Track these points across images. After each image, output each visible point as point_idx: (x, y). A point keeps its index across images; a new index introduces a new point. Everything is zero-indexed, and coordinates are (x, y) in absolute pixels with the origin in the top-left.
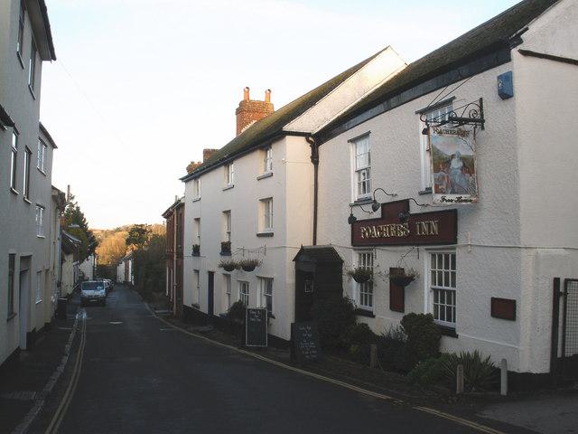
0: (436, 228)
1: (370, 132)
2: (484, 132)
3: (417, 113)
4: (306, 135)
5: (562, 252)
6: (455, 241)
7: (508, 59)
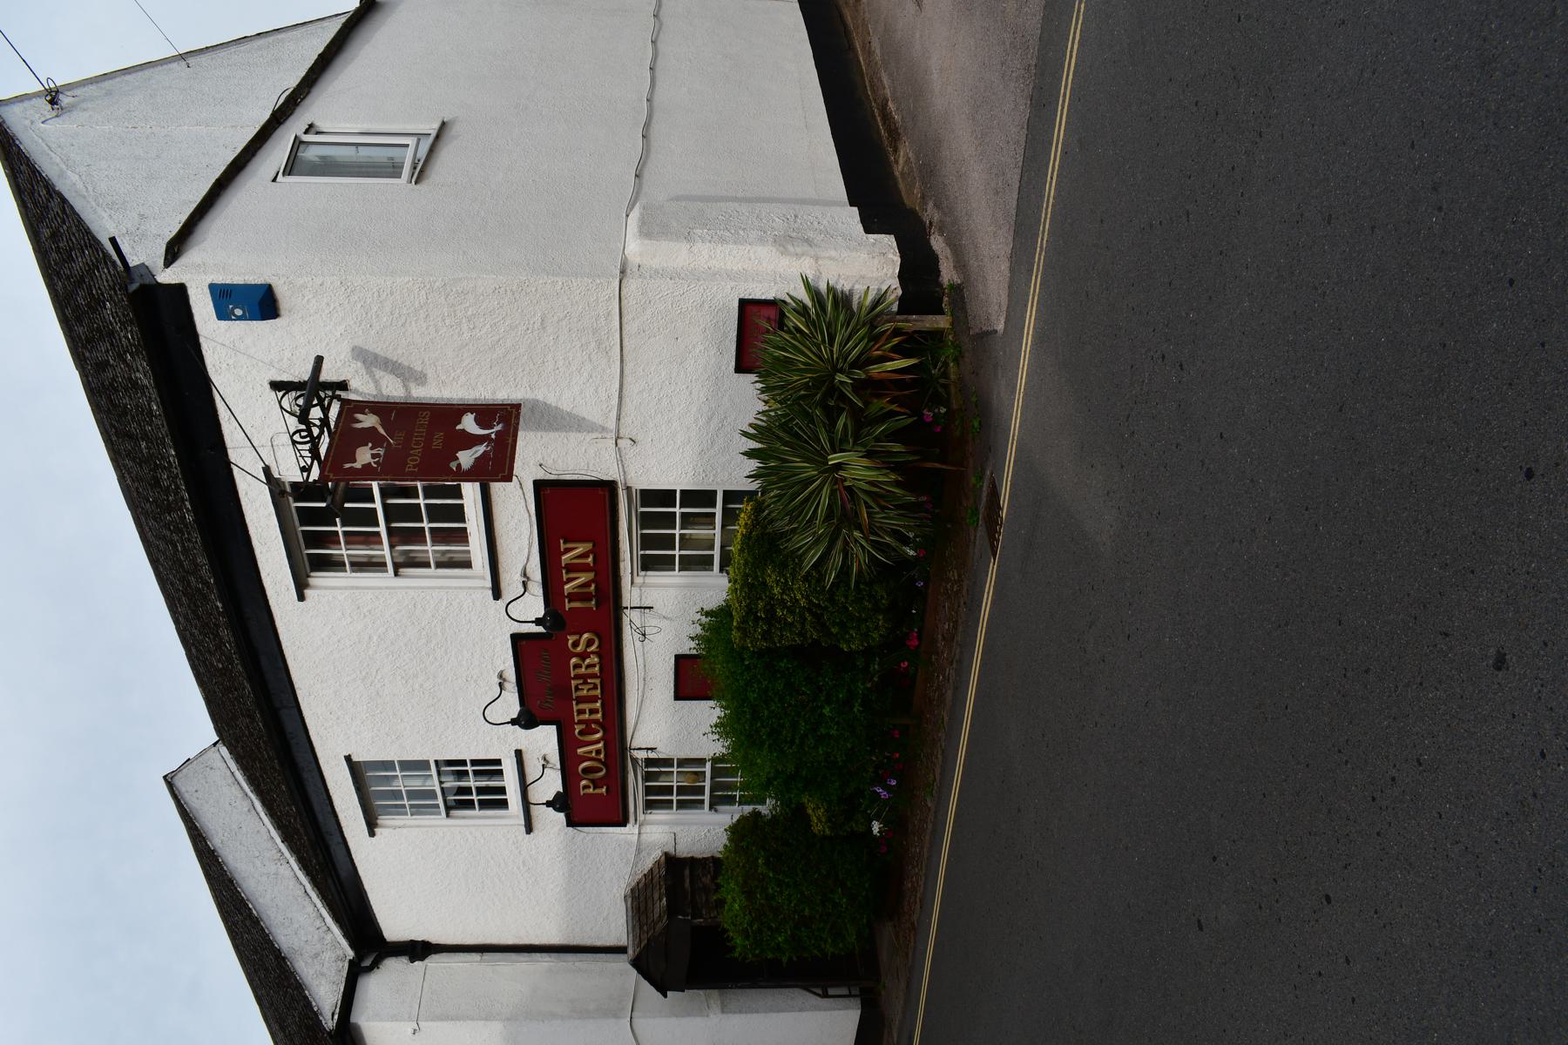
0: (581, 548)
1: (348, 759)
2: (353, 384)
3: (301, 597)
4: (355, 973)
5: (635, 214)
6: (610, 487)
7: (181, 290)
